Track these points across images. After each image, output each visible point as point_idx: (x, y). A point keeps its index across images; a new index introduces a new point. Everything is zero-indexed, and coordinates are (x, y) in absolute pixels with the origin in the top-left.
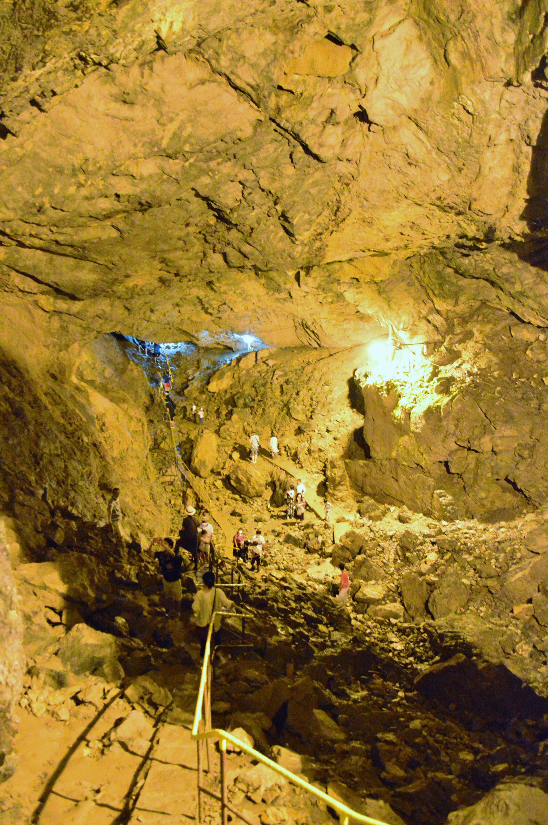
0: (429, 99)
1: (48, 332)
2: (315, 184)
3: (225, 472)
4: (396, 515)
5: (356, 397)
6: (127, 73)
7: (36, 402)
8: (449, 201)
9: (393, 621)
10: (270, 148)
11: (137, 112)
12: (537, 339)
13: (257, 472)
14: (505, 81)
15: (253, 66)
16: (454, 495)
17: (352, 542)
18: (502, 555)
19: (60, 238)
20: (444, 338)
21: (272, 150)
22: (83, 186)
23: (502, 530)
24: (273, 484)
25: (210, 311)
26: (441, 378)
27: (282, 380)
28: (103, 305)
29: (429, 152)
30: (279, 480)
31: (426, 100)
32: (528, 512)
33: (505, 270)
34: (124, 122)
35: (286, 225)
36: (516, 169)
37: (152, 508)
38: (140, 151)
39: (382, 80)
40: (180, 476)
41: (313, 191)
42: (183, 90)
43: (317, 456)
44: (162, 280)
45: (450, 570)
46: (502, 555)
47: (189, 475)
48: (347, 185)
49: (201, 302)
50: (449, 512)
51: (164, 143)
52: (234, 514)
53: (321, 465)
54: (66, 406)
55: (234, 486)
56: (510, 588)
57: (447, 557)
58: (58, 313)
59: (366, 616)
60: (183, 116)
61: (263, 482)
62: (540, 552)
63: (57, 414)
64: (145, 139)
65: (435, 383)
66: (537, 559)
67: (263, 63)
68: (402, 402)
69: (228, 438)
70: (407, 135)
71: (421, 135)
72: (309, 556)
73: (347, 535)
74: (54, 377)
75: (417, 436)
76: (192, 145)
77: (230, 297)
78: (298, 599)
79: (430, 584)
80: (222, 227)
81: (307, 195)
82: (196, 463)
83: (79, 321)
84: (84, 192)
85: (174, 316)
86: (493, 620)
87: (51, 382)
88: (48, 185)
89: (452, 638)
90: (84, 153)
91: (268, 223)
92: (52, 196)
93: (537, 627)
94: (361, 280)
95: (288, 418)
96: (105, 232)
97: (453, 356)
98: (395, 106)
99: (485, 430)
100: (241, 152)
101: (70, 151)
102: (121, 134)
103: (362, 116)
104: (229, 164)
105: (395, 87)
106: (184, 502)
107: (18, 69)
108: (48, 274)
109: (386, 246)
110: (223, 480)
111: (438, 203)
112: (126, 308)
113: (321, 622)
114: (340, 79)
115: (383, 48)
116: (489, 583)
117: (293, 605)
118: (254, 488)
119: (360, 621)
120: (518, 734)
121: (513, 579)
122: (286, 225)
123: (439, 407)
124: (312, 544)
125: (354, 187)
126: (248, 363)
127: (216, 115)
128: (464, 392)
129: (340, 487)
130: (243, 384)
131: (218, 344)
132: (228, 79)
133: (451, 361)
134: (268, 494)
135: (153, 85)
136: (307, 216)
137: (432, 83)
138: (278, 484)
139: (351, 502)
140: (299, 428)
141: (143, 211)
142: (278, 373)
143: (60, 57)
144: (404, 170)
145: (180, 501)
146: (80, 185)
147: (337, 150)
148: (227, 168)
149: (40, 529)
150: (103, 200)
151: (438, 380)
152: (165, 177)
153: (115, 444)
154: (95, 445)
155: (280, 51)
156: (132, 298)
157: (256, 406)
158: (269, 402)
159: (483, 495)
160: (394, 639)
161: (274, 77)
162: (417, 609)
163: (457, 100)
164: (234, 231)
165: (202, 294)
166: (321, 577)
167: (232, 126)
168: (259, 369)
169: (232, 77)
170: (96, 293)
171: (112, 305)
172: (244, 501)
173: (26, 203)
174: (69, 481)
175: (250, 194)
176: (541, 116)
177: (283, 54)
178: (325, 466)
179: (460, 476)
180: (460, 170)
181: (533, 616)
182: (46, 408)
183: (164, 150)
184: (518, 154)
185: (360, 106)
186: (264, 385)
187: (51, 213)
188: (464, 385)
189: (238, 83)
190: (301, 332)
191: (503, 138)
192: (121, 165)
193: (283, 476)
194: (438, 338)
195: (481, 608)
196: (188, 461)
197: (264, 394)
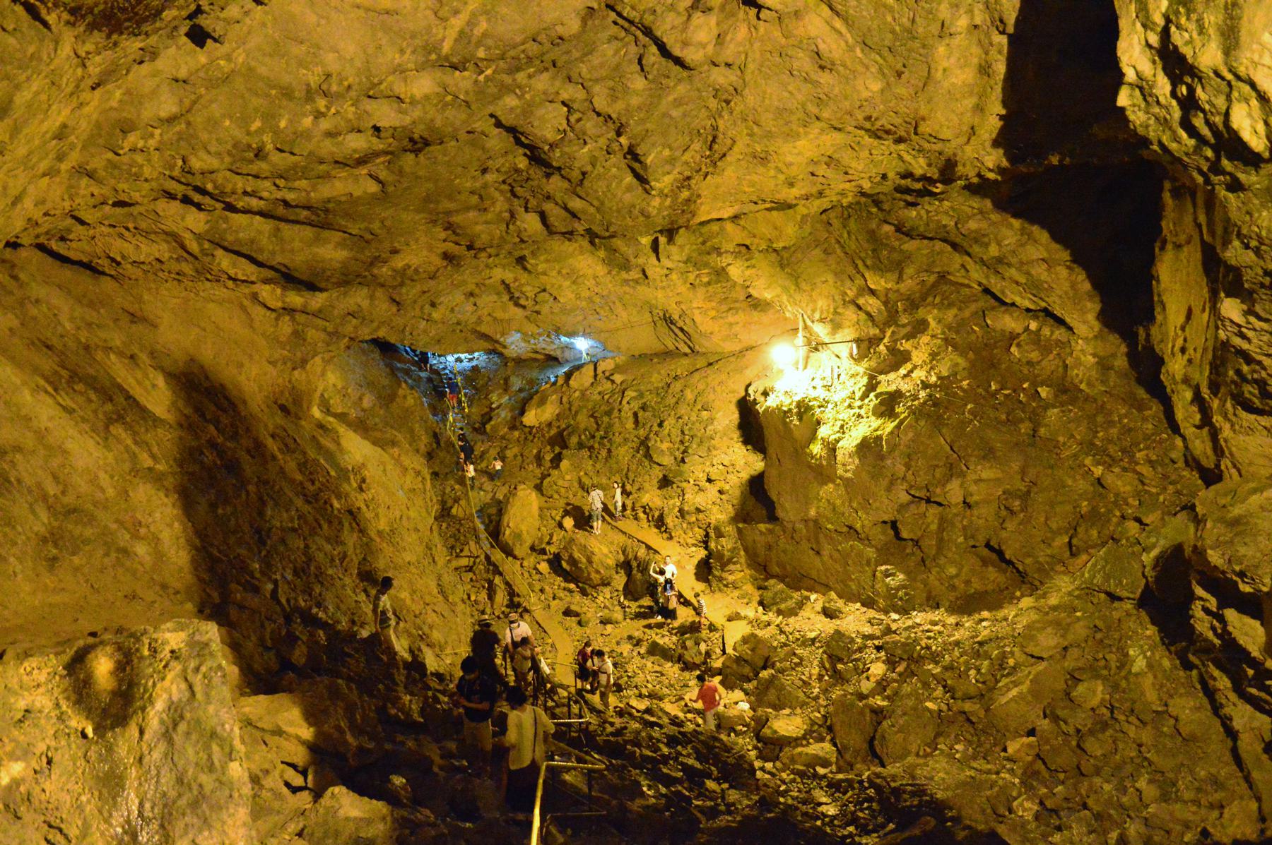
2: (678, 103)
3: (553, 549)
4: (819, 607)
5: (752, 425)
7: (258, 449)
9: (821, 771)
10: (608, 50)
12: (1027, 329)
13: (602, 546)
17: (753, 650)
18: (986, 663)
19: (290, 196)
20: (883, 332)
21: (610, 53)
23: (984, 625)
24: (626, 566)
25: (522, 302)
26: (881, 394)
27: (636, 405)
28: (358, 298)
30: (636, 558)
32: (1023, 596)
33: (973, 225)
35: (636, 166)
36: (985, 70)
37: (442, 607)
38: (409, 59)
40: (483, 557)
41: (674, 113)
43: (694, 519)
45: (907, 689)
46: (986, 663)
47: (497, 556)
48: (728, 102)
49: (507, 287)
50: (901, 599)
51: (446, 47)
52: (568, 613)
53: (699, 533)
55: (569, 570)
57: (900, 669)
58: (290, 311)
59: (778, 764)
61: (611, 562)
63: (291, 466)
65: (872, 400)
66: (1041, 666)
68: (823, 432)
69: (556, 496)
71: (838, 24)
72: (687, 674)
73: (745, 640)
75: (848, 483)
76: (488, 48)
78: (672, 741)
79: (878, 712)
80: (537, 173)
81: (667, 120)
84: (325, 124)
85: (467, 312)
86: (974, 764)
88: (270, 118)
89: (913, 794)
92: (276, 132)
93: (1045, 773)
94: (753, 248)
95: (647, 463)
97: (898, 359)
99: (952, 471)
100: (565, 58)
102: (380, 34)
104: (546, 75)
106: (491, 597)
108: (273, 253)
109: (791, 194)
110: (549, 561)
111: (868, 125)
113: (709, 776)
116: (967, 706)
117: (665, 750)
118: (598, 572)
119: (769, 773)
121: (1004, 700)
122: (636, 166)
123: (879, 438)
126: (583, 379)
128: (917, 413)
129: (731, 567)
130: (576, 413)
133: (895, 367)
134: (620, 580)
136: (667, 152)
138: (634, 564)
139: (749, 588)
140: (665, 476)
141: (416, 152)
142: (630, 394)
144: (814, 77)
145: (483, 595)
146: (319, 115)
147: (710, 49)
148: (543, 82)
149: (269, 643)
151: (877, 396)
152: (449, 98)
154: (350, 512)
156: (402, 284)
157: (596, 446)
158: (618, 439)
159: (952, 571)
160: (824, 800)
164: (555, 179)
167: (550, 17)
168: (600, 389)
170: (346, 279)
171: (372, 297)
172: (584, 593)
175: (579, 120)
178: (707, 535)
179: (916, 543)
180: (899, 74)
181: (1038, 755)
182: (274, 458)
183: (446, 58)
184: (986, 47)
186: (609, 413)
187: (276, 157)
188: (916, 403)
193: (642, 552)
194: (874, 331)
195: (957, 747)
196: (495, 532)
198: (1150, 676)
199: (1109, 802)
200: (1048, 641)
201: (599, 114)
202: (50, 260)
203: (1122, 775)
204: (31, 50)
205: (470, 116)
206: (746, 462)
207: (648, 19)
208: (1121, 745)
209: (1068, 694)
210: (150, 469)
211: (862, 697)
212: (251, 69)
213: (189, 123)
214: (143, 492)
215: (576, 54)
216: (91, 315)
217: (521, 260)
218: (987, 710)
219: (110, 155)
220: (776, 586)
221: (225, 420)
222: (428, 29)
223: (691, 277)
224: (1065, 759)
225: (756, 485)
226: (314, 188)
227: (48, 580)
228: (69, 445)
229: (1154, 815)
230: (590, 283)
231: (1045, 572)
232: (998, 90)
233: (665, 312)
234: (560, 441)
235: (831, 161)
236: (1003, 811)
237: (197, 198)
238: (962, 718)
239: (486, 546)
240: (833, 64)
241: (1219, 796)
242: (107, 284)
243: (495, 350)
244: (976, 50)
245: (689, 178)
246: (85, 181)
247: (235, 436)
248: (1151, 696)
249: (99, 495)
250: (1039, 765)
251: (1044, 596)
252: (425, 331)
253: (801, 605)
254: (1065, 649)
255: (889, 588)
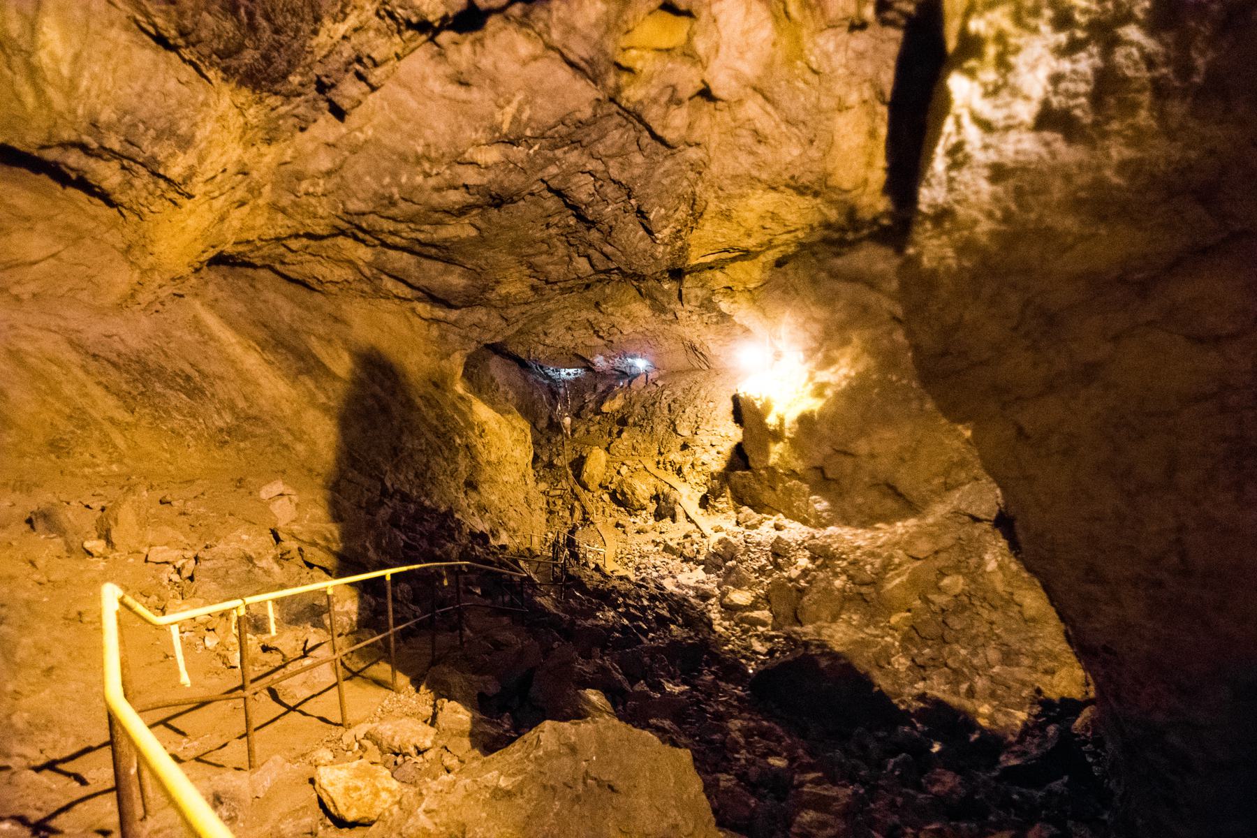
0: (773, 62)
1: (427, 339)
2: (667, 174)
3: (613, 487)
5: (740, 411)
6: (459, 51)
7: (409, 404)
8: (804, 180)
10: (615, 135)
11: (475, 94)
13: (643, 489)
14: (847, 23)
15: (585, 38)
16: (830, 500)
19: (421, 236)
21: (617, 136)
22: (430, 176)
23: (884, 533)
24: (656, 498)
27: (670, 400)
28: (480, 314)
29: (778, 126)
31: (769, 66)
34: (461, 105)
35: (645, 221)
36: (872, 134)
37: (524, 510)
38: (481, 136)
39: (723, 49)
41: (666, 182)
42: (515, 68)
44: (533, 288)
47: (578, 489)
48: (700, 173)
49: (591, 324)
51: (505, 127)
52: (618, 525)
54: (442, 409)
55: (622, 500)
56: (888, 595)
57: (819, 562)
58: (437, 321)
60: (520, 97)
61: (648, 495)
62: (921, 556)
63: (431, 415)
64: (485, 123)
65: (811, 387)
66: (918, 563)
67: (596, 35)
70: (753, 108)
71: (769, 108)
72: (684, 565)
73: (720, 542)
74: (436, 385)
76: (533, 129)
77: (617, 318)
78: (652, 598)
79: (801, 591)
80: (582, 227)
81: (660, 187)
82: (585, 476)
83: (457, 330)
84: (432, 182)
85: (568, 341)
86: (867, 631)
87: (431, 389)
88: (395, 175)
89: (818, 646)
90: (425, 139)
91: (626, 220)
92: (400, 186)
93: (917, 638)
96: (460, 230)
97: (829, 362)
98: (738, 76)
99: (862, 433)
100: (587, 139)
101: (411, 136)
102: (460, 118)
103: (706, 93)
104: (576, 152)
105: (737, 55)
106: (571, 515)
107: (318, 19)
108: (418, 278)
109: (749, 243)
111: (792, 183)
112: (503, 317)
113: (674, 623)
114: (678, 51)
115: (721, 11)
116: (864, 590)
117: (646, 603)
120: (864, 747)
121: (889, 586)
122: (645, 221)
124: (686, 552)
125: (707, 175)
126: (639, 383)
127: (552, 95)
128: (839, 395)
129: (721, 499)
131: (613, 369)
132: (562, 55)
134: (652, 507)
135: (486, 63)
136: (663, 211)
137: (774, 44)
141: (498, 206)
142: (667, 392)
143: (362, 8)
144: (754, 149)
145: (567, 513)
146: (427, 175)
147: (683, 132)
148: (574, 157)
149: (364, 505)
150: (451, 192)
152: (511, 166)
153: (493, 449)
154: (467, 446)
155: (612, 21)
156: (507, 307)
158: (656, 420)
159: (860, 500)
161: (609, 51)
162: (786, 618)
163: (801, 57)
164: (593, 231)
165: (591, 317)
166: (692, 583)
167: (571, 105)
169: (565, 51)
170: (470, 301)
171: (488, 314)
173: (375, 193)
174: (429, 474)
175: (601, 186)
176: (892, 63)
177: (616, 24)
179: (836, 481)
180: (812, 142)
182: (419, 409)
183: (506, 135)
184: (872, 114)
185: (703, 81)
186: (653, 405)
187: (403, 205)
189: (572, 57)
190: (691, 355)
191: (853, 98)
192: (464, 153)
193: (666, 489)
196: (578, 476)
197: (653, 413)
198: (1000, 575)
199: (963, 662)
200: (924, 546)
201: (614, 182)
202: (280, 279)
203: (974, 644)
204: (201, 98)
205: (528, 179)
206: (735, 434)
207: (639, 108)
208: (976, 623)
209: (936, 584)
210: (324, 404)
211: (790, 580)
212: (378, 140)
213: (342, 177)
214: (311, 415)
215: (594, 136)
216: (305, 314)
217: (597, 305)
218: (878, 593)
219: (293, 197)
220: (746, 510)
221: (388, 383)
222: (492, 115)
223: (705, 318)
224: (932, 630)
225: (739, 450)
226: (435, 231)
227: (217, 454)
228: (262, 381)
229: (998, 674)
230: (642, 322)
231: (926, 503)
232: (882, 146)
233: (691, 342)
234: (623, 422)
235: (774, 216)
236: (883, 663)
237: (361, 235)
238: (859, 598)
239: (571, 482)
240: (766, 138)
241: (1050, 664)
242: (319, 298)
243: (589, 367)
244: (866, 120)
245: (679, 231)
246: (280, 216)
247: (393, 394)
248: (1000, 587)
249: (279, 413)
250: (913, 633)
251: (924, 517)
252: (543, 352)
253: (761, 522)
254: (936, 552)
255: (817, 512)
